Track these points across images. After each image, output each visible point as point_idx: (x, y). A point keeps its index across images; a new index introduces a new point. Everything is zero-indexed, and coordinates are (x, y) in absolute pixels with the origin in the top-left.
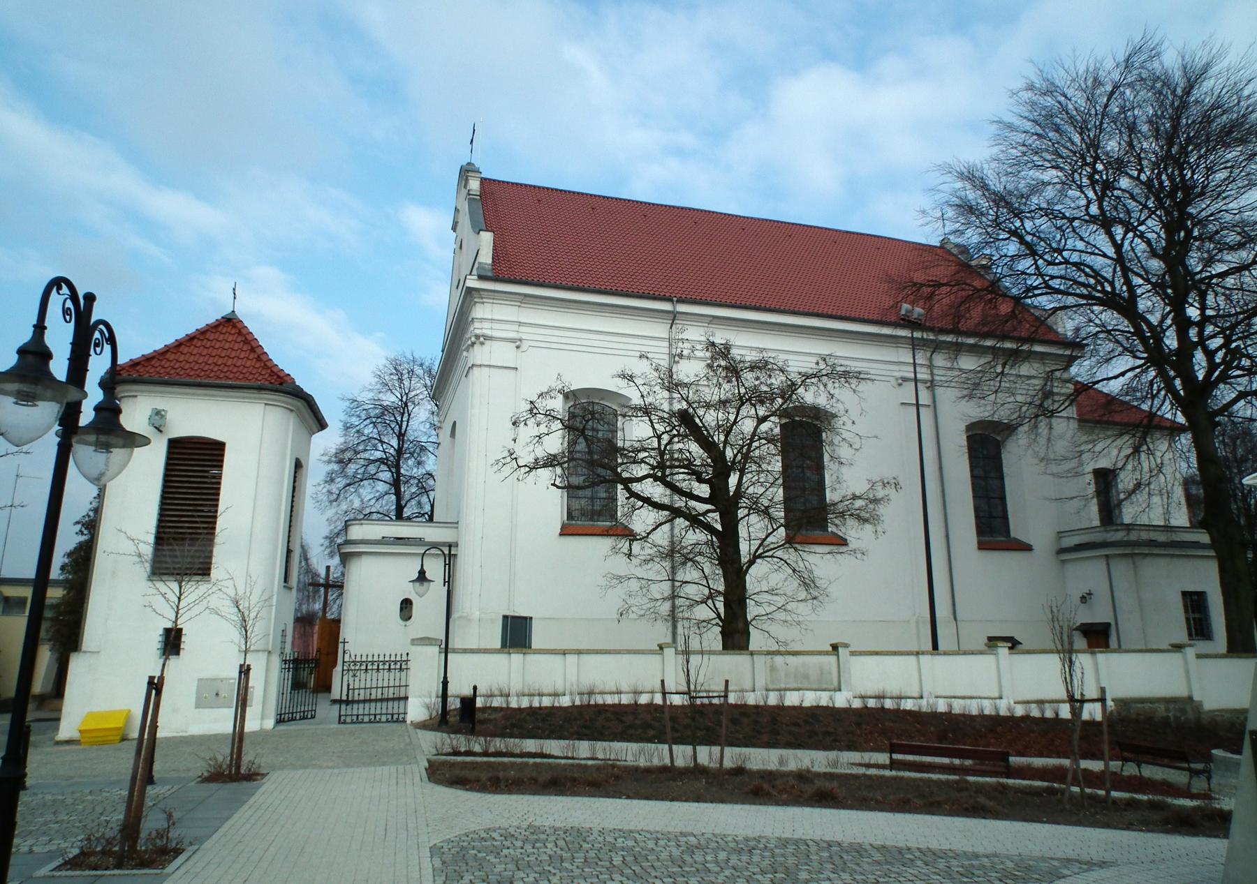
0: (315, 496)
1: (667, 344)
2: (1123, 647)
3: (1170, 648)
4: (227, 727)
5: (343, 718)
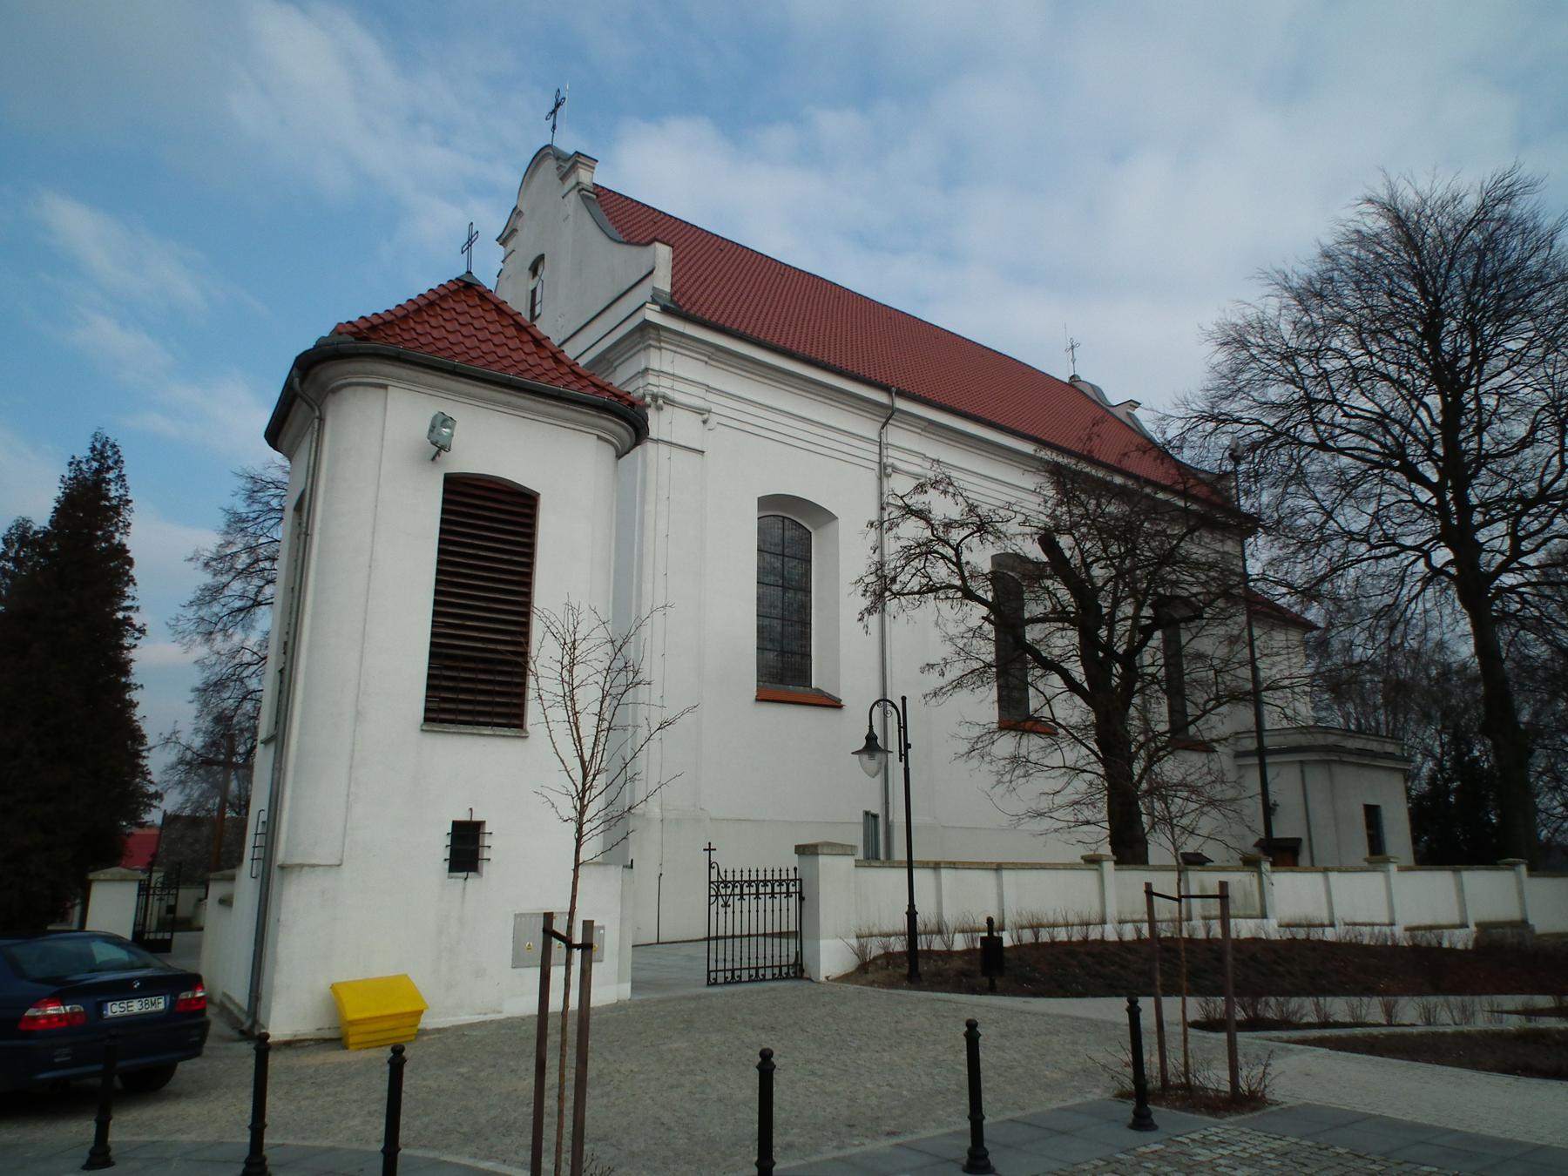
0: (173, 623)
1: (877, 449)
2: (1317, 864)
3: (1366, 864)
4: (531, 1006)
5: (713, 975)
